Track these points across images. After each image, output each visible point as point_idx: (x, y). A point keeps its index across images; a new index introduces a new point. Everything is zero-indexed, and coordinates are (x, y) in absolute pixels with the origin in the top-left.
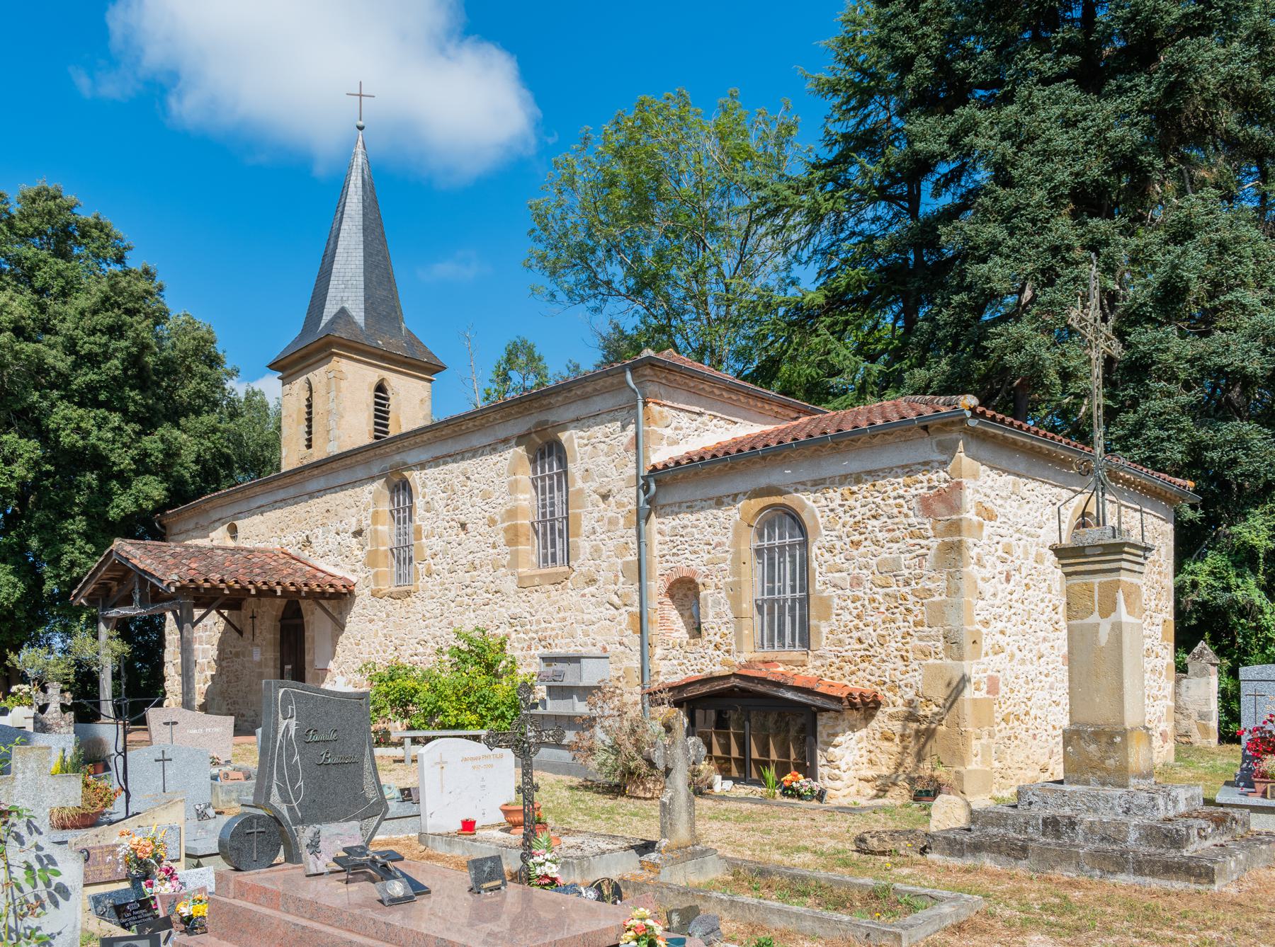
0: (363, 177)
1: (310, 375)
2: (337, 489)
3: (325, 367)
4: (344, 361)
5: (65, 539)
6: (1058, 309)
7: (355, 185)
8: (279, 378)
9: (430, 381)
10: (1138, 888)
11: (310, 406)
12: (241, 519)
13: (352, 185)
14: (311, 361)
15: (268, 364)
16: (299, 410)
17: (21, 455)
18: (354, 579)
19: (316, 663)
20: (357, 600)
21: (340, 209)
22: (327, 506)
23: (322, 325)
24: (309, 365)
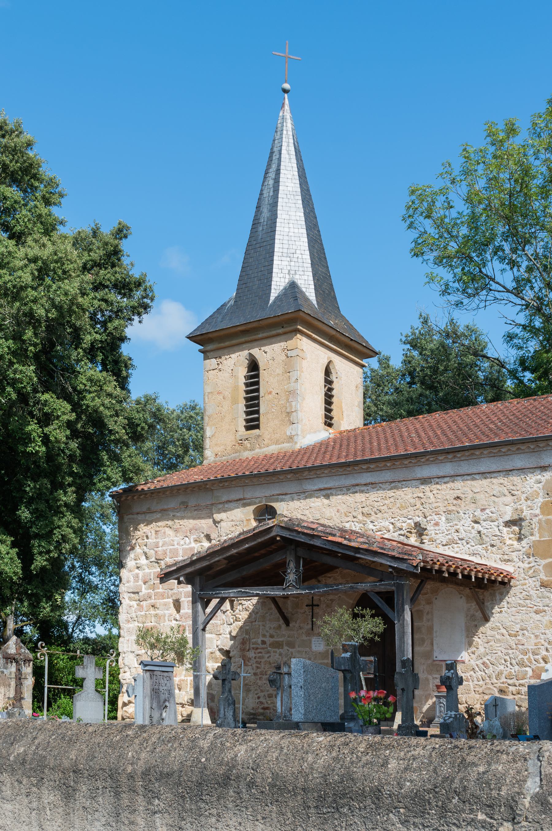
0: (294, 144)
1: (256, 352)
2: (477, 477)
3: (283, 344)
4: (304, 339)
5: (58, 512)
6: (43, 358)
7: (288, 151)
8: (200, 351)
9: (362, 366)
10: (437, 790)
11: (328, 382)
12: (282, 500)
13: (284, 152)
14: (260, 336)
15: (187, 333)
16: (236, 388)
17: (58, 417)
18: (509, 568)
19: (435, 654)
20: (512, 592)
21: (272, 175)
22: (458, 493)
23: (272, 298)
24: (256, 340)
